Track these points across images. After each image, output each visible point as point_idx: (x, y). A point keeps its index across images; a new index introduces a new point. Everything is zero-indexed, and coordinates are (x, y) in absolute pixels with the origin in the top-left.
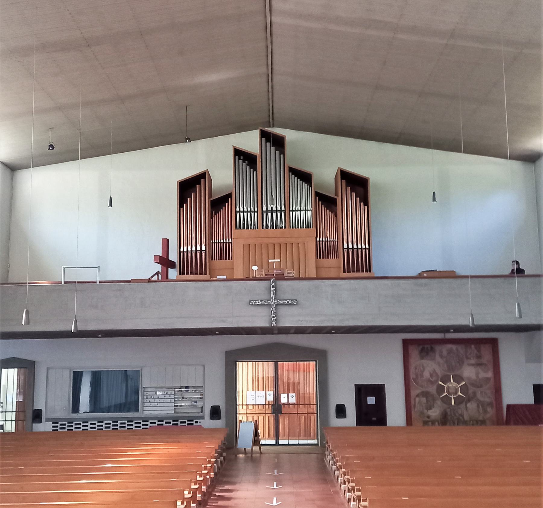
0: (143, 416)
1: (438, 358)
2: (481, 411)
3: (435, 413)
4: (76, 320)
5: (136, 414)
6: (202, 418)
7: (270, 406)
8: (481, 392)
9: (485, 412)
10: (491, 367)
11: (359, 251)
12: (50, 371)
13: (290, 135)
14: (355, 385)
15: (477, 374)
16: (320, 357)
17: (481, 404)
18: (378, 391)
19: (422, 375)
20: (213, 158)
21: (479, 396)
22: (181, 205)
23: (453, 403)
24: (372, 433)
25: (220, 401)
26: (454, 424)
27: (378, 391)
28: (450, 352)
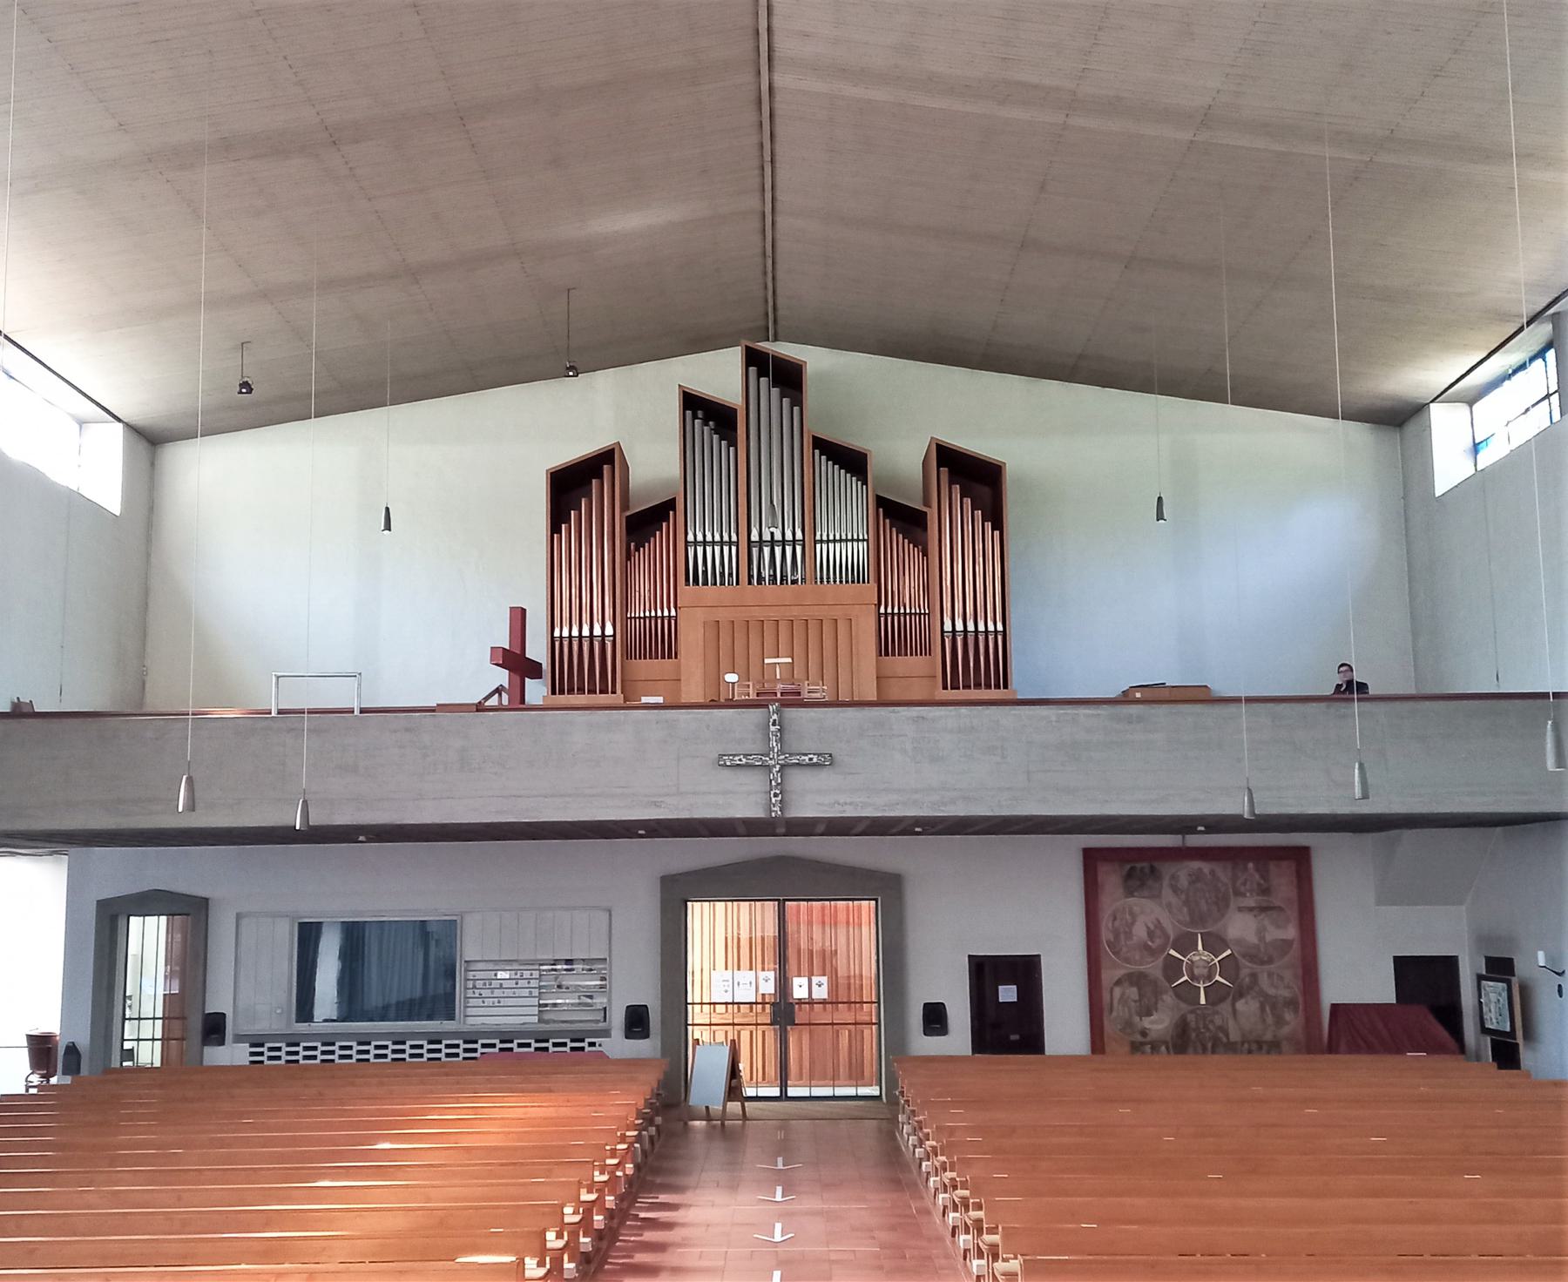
1: (1167, 892)
2: (1270, 1019)
3: (1159, 1024)
5: (448, 1026)
6: (606, 1033)
8: (1270, 975)
9: (1280, 1021)
10: (1293, 913)
11: (981, 638)
12: (244, 922)
13: (815, 360)
14: (970, 957)
15: (1261, 932)
17: (1268, 1002)
18: (1025, 970)
19: (1129, 935)
20: (630, 414)
21: (1264, 981)
22: (555, 528)
23: (1203, 1001)
24: (1010, 1070)
25: (648, 995)
27: (1025, 970)
28: (1196, 877)
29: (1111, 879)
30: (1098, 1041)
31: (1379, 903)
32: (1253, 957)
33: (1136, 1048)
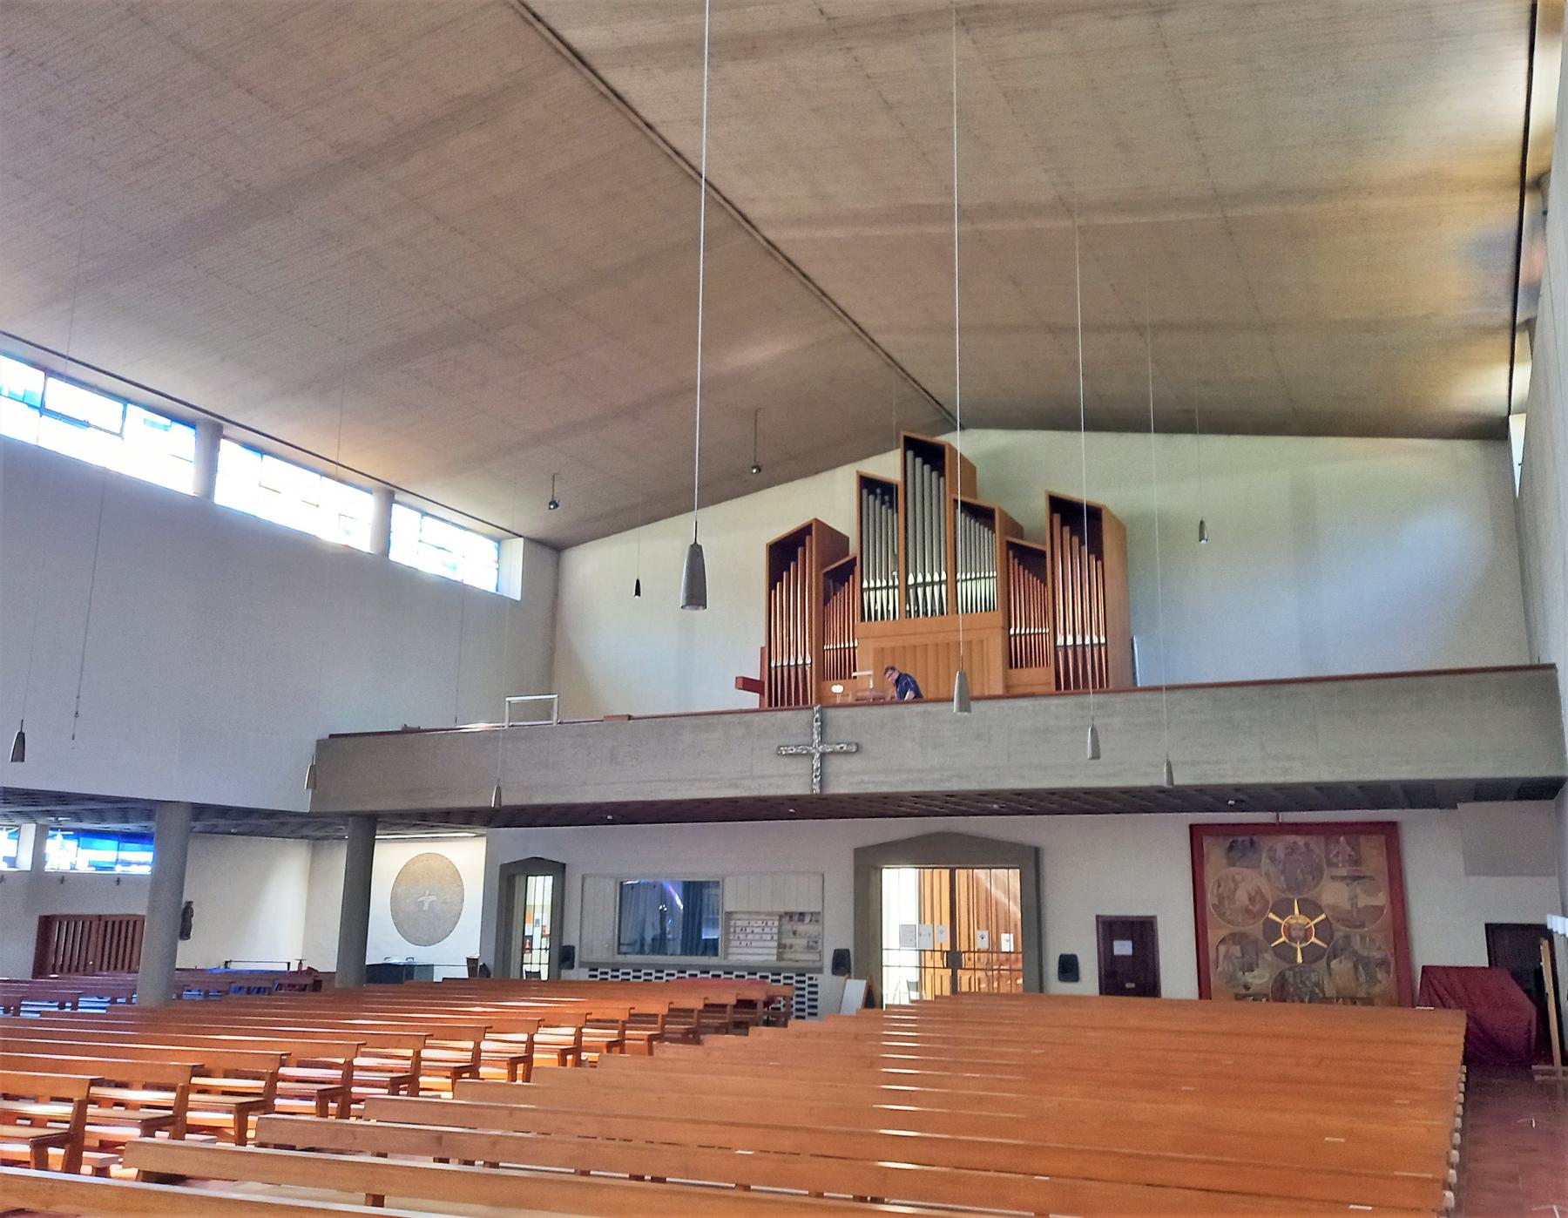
0: (724, 962)
1: (1265, 860)
2: (1362, 979)
3: (1260, 979)
4: (499, 789)
5: (713, 960)
6: (820, 970)
7: (938, 955)
8: (1363, 938)
9: (1372, 980)
10: (1383, 880)
11: (1088, 650)
12: (588, 881)
13: (960, 442)
14: (1098, 917)
15: (1353, 899)
16: (1030, 862)
17: (1360, 962)
18: (1142, 931)
19: (1232, 899)
20: (830, 499)
21: (1356, 943)
22: (772, 586)
23: (1300, 960)
24: (1132, 1010)
25: (847, 943)
26: (1302, 1001)
27: (1142, 931)
28: (1292, 849)
29: (1215, 853)
30: (1204, 989)
31: (1469, 873)
32: (1346, 920)
33: (1238, 997)
